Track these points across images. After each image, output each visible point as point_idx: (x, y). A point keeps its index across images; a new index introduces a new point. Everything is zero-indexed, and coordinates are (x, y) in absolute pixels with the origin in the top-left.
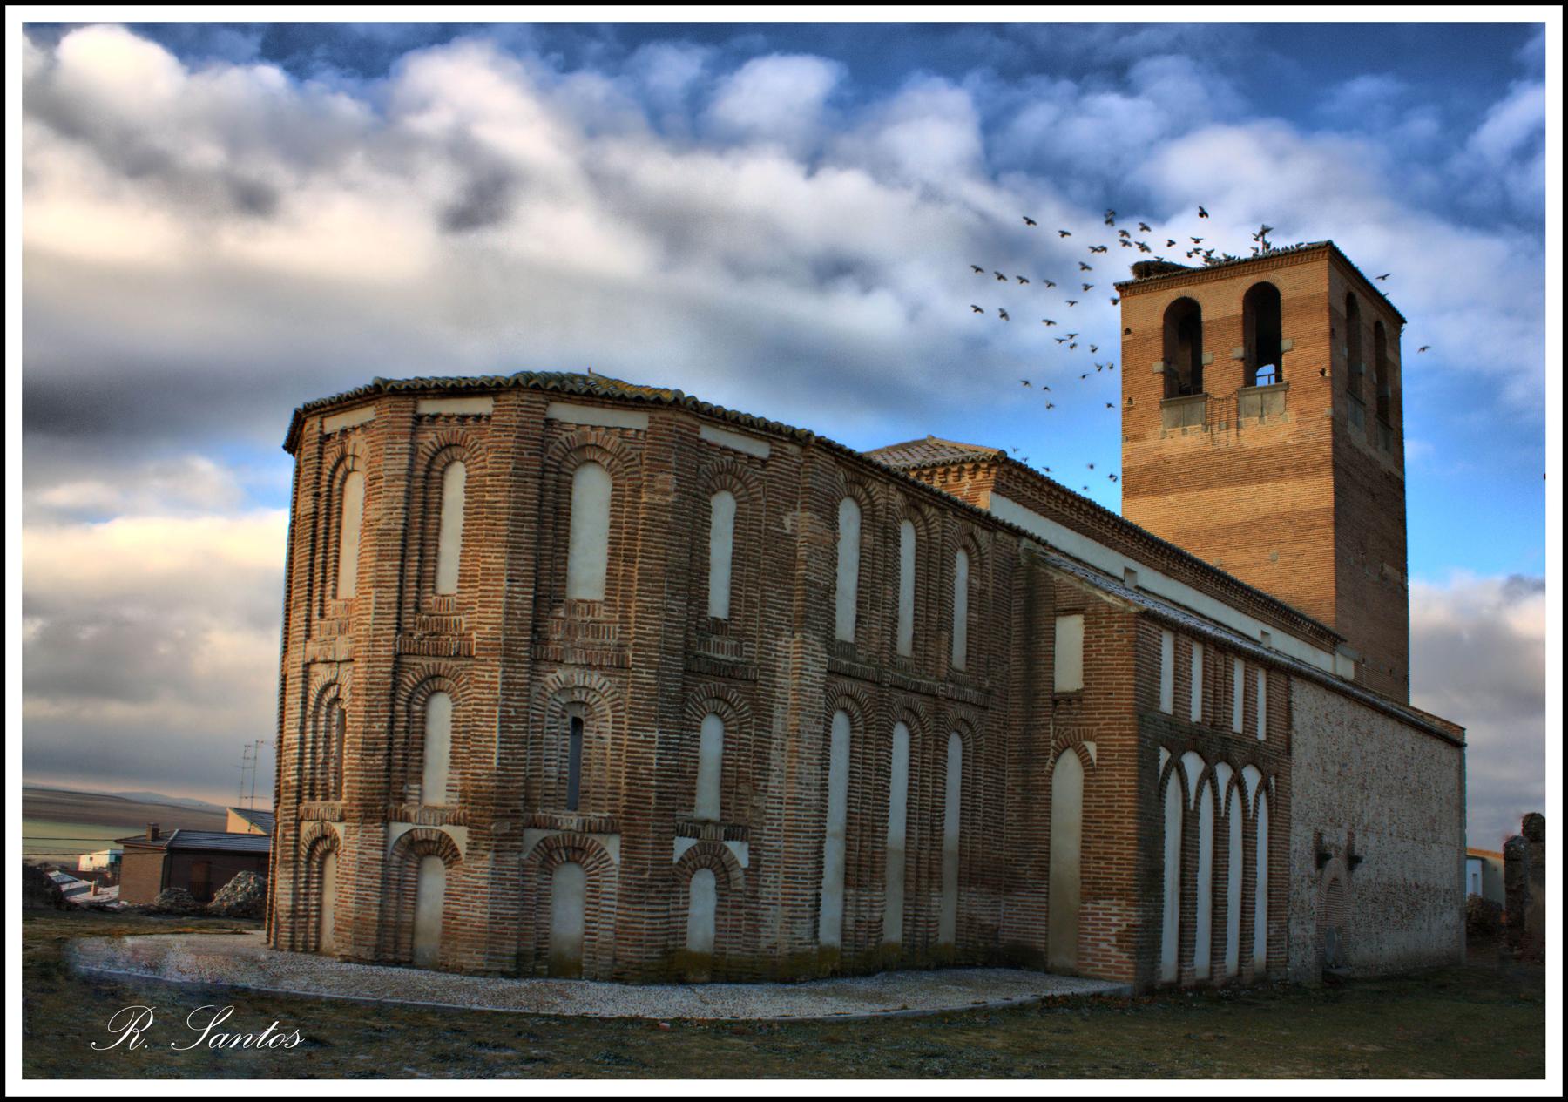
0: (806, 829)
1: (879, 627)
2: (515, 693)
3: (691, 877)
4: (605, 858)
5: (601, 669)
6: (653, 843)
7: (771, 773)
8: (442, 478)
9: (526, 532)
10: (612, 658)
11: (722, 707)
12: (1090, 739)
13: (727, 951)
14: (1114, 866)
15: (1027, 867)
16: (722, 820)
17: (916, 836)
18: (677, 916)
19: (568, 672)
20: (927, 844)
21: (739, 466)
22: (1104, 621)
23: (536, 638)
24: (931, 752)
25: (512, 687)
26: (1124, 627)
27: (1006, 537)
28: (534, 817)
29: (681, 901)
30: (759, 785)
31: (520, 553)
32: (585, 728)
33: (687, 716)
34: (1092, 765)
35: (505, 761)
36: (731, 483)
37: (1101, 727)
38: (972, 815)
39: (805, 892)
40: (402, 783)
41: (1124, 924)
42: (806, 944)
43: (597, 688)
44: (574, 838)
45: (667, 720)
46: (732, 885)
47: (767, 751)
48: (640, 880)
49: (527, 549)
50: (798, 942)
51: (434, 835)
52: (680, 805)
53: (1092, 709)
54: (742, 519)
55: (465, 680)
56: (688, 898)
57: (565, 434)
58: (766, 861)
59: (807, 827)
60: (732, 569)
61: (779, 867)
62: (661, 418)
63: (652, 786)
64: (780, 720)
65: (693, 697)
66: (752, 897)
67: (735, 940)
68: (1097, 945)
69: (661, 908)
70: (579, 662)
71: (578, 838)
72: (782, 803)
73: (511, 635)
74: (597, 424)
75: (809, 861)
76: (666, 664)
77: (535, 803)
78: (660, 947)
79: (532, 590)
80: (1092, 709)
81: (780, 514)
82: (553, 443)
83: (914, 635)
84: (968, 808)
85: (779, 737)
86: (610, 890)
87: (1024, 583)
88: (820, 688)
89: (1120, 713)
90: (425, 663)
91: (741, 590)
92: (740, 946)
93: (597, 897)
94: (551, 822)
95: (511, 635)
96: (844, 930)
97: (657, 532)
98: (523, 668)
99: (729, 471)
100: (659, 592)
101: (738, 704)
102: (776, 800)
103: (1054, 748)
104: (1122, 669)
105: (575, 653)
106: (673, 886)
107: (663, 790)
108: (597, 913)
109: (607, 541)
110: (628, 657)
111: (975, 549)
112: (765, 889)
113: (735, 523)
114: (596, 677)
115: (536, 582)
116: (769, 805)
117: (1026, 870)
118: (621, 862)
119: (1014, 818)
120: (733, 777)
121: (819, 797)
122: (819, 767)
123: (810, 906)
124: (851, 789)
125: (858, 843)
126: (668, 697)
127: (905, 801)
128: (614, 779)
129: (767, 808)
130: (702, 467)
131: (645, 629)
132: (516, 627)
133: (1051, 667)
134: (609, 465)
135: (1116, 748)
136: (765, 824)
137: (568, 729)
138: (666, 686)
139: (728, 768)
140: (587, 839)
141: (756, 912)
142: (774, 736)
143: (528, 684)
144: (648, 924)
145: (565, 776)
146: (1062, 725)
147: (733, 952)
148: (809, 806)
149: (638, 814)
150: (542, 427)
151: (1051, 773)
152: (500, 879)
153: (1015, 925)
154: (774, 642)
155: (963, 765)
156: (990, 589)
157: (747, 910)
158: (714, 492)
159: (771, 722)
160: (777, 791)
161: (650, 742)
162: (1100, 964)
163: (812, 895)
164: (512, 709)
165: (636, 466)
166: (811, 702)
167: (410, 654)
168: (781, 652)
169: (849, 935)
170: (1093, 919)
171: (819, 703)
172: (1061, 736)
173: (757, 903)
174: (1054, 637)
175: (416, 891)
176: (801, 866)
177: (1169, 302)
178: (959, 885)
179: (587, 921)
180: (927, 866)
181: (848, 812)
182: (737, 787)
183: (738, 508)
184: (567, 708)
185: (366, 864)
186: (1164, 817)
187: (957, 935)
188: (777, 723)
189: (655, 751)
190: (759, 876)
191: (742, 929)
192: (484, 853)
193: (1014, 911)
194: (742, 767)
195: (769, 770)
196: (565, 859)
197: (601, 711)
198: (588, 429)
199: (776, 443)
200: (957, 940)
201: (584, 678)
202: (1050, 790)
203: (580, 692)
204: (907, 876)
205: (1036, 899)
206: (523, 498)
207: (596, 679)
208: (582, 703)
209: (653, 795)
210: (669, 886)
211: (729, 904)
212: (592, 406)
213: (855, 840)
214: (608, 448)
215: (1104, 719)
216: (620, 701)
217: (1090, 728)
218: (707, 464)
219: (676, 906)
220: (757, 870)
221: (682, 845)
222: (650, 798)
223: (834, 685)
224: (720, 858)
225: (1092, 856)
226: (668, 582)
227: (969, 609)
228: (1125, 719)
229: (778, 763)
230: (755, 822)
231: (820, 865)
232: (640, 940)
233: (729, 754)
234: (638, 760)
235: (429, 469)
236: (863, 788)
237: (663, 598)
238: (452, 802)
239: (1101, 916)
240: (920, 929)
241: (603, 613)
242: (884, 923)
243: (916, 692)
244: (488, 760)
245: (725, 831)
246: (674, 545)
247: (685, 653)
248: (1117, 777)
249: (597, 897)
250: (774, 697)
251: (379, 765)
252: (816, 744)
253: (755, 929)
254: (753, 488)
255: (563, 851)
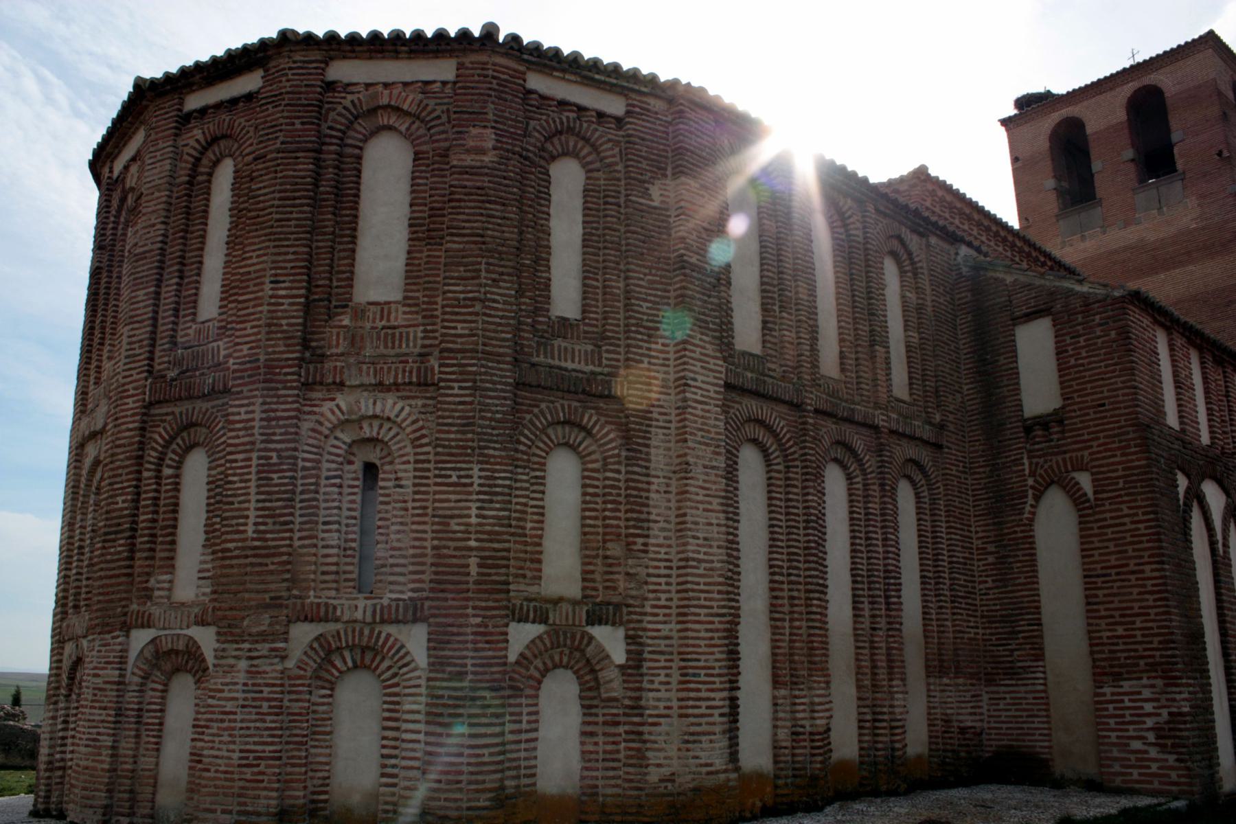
0: (707, 603)
1: (793, 335)
2: (278, 431)
3: (540, 682)
4: (405, 661)
5: (398, 390)
6: (475, 633)
7: (651, 525)
8: (209, 181)
9: (297, 219)
10: (411, 372)
11: (575, 436)
12: (1081, 469)
13: (600, 790)
14: (1138, 633)
15: (1014, 647)
16: (585, 597)
17: (867, 613)
18: (519, 742)
19: (351, 399)
20: (882, 622)
21: (585, 125)
22: (1080, 316)
23: (307, 355)
24: (877, 500)
25: (274, 423)
26: (1109, 318)
27: (941, 243)
28: (303, 605)
29: (525, 718)
30: (635, 543)
31: (287, 246)
32: (381, 476)
33: (522, 448)
34: (1088, 501)
35: (262, 528)
36: (575, 146)
37: (1095, 449)
38: (937, 583)
39: (712, 695)
40: (148, 574)
41: (1165, 712)
42: (717, 772)
43: (392, 416)
44: (361, 633)
45: (491, 452)
46: (602, 690)
47: (644, 494)
48: (455, 689)
49: (296, 240)
50: (705, 770)
51: (181, 642)
52: (516, 576)
53: (1079, 429)
54: (593, 191)
55: (220, 425)
56: (537, 713)
57: (350, 97)
58: (650, 652)
59: (711, 600)
60: (584, 253)
61: (671, 660)
62: (472, 63)
63: (470, 549)
64: (661, 451)
65: (531, 421)
66: (632, 708)
67: (611, 773)
68: (1128, 745)
69: (489, 730)
70: (366, 380)
71: (366, 632)
72: (670, 568)
73: (274, 353)
74: (390, 80)
75: (716, 650)
76: (485, 374)
77: (304, 584)
78: (490, 790)
79: (303, 292)
80: (1079, 429)
81: (644, 182)
82: (335, 109)
83: (841, 352)
84: (930, 575)
85: (660, 474)
86: (415, 707)
87: (969, 294)
88: (717, 406)
89: (1119, 428)
90: (177, 410)
91: (597, 280)
92: (619, 782)
93: (396, 720)
94: (327, 612)
95: (274, 353)
96: (776, 747)
97: (470, 201)
98: (289, 396)
99: (570, 130)
100: (473, 278)
101: (599, 431)
102: (662, 564)
103: (1032, 487)
104: (1114, 371)
105: (360, 370)
106: (509, 697)
107: (487, 554)
108: (397, 743)
109: (406, 223)
110: (433, 369)
111: (905, 257)
112: (651, 695)
113: (585, 196)
114: (390, 402)
115: (309, 282)
116: (651, 571)
117: (1012, 651)
118: (430, 664)
119: (990, 585)
120: (598, 534)
121: (725, 558)
122: (722, 515)
123: (721, 715)
124: (772, 548)
125: (787, 624)
126: (491, 419)
127: (849, 566)
128: (417, 543)
129: (648, 575)
130: (532, 123)
131: (455, 328)
132: (281, 342)
133: (1017, 390)
134: (408, 129)
135: (1120, 473)
136: (646, 599)
137: (357, 479)
138: (488, 405)
139: (589, 522)
140: (380, 633)
141: (641, 729)
142: (653, 473)
143: (296, 417)
144: (470, 756)
145: (353, 545)
146: (1039, 457)
147: (609, 791)
148: (711, 569)
149: (451, 591)
150: (319, 90)
151: (1032, 520)
152: (254, 699)
153: (1004, 726)
154: (646, 345)
155: (919, 520)
156: (929, 303)
157: (627, 728)
158: (553, 158)
159: (648, 454)
160: (663, 550)
161: (465, 485)
162: (1135, 772)
163: (724, 699)
164: (274, 454)
165: (443, 124)
166: (703, 424)
167: (167, 401)
168: (657, 358)
169: (785, 755)
170: (1115, 709)
171: (715, 426)
172: (1039, 471)
173: (642, 715)
174: (1015, 351)
175: (161, 724)
176: (703, 657)
177: (1053, 125)
178: (928, 677)
179: (383, 756)
180: (884, 651)
181: (772, 581)
182: (605, 549)
183: (588, 178)
184: (355, 450)
185: (100, 689)
186: (1194, 562)
187: (930, 743)
188: (657, 455)
189: (475, 497)
190: (642, 675)
191: (621, 756)
192: (232, 661)
193: (1001, 707)
194: (610, 518)
195: (648, 521)
196: (350, 664)
197: (400, 449)
198: (380, 88)
199: (633, 96)
200: (931, 750)
201: (375, 403)
202: (1034, 543)
203: (371, 425)
204: (859, 667)
205: (1030, 688)
206: (294, 177)
207: (390, 405)
208: (373, 441)
209: (473, 561)
210: (502, 697)
211: (601, 719)
212: (383, 58)
213: (783, 620)
214: (405, 107)
215: (1098, 438)
216: (424, 432)
217: (1079, 454)
218: (539, 120)
219: (516, 726)
220: (639, 667)
221: (522, 635)
222: (468, 566)
223: (736, 406)
224: (583, 652)
225: (1103, 622)
226: (487, 264)
227: (906, 327)
228: (1128, 433)
229: (662, 511)
230: (632, 597)
231: (733, 656)
232: (459, 782)
233: (590, 502)
234: (449, 512)
235: (193, 173)
236: (788, 547)
237: (480, 285)
238: (204, 594)
239: (1128, 704)
240: (880, 739)
241: (400, 316)
242: (832, 734)
243: (849, 420)
244: (242, 528)
245: (588, 612)
246: (493, 216)
247: (516, 360)
248: (1126, 511)
249: (396, 720)
250: (651, 419)
251: (119, 553)
252: (715, 483)
253: (640, 755)
254: (606, 150)
255: (347, 654)
